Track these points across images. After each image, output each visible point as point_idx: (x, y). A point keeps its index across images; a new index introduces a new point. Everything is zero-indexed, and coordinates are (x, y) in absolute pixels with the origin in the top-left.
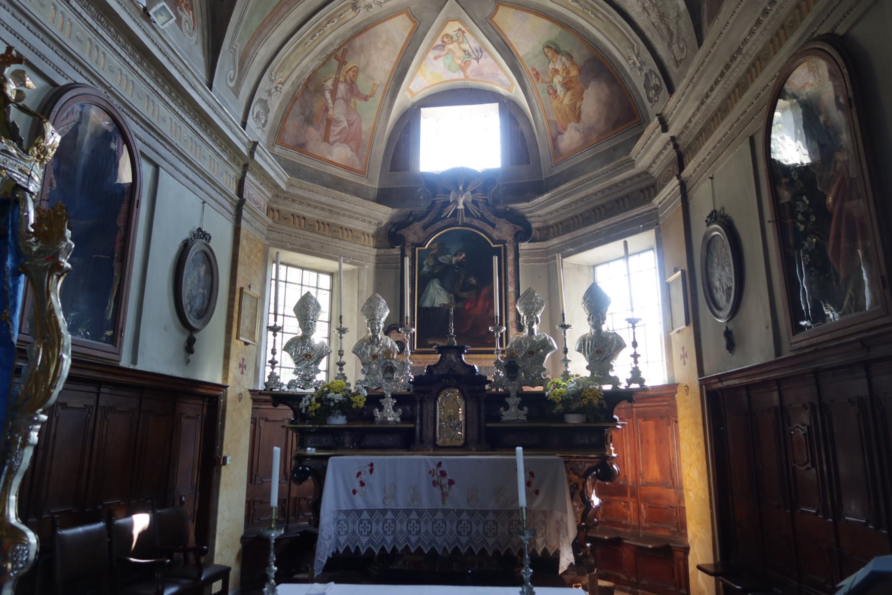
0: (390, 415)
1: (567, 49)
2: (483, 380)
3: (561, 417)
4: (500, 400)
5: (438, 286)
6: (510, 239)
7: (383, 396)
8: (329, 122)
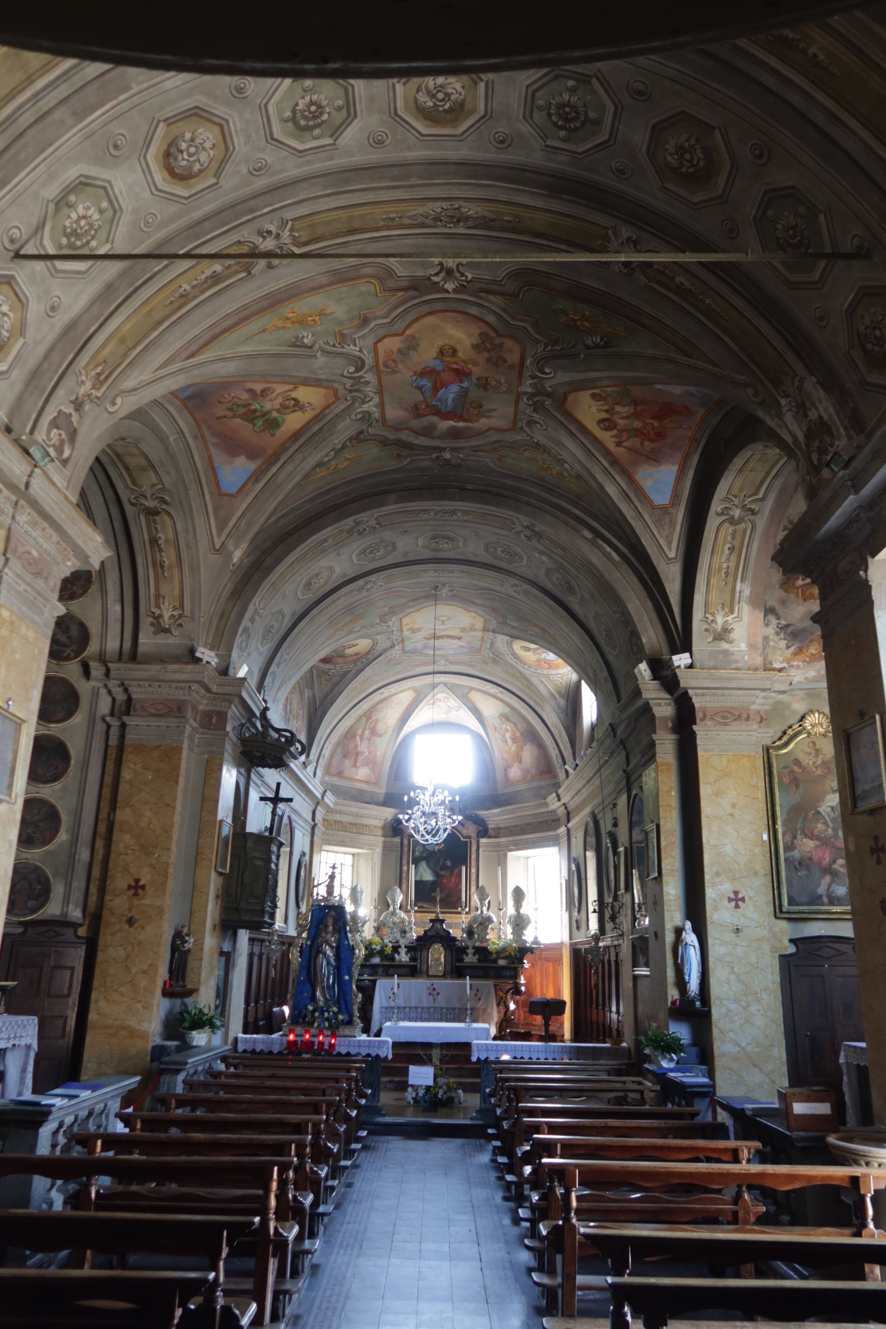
0: (403, 957)
1: (514, 720)
2: (454, 939)
3: (495, 961)
4: (463, 950)
5: (425, 866)
6: (474, 835)
7: (400, 947)
8: (357, 754)
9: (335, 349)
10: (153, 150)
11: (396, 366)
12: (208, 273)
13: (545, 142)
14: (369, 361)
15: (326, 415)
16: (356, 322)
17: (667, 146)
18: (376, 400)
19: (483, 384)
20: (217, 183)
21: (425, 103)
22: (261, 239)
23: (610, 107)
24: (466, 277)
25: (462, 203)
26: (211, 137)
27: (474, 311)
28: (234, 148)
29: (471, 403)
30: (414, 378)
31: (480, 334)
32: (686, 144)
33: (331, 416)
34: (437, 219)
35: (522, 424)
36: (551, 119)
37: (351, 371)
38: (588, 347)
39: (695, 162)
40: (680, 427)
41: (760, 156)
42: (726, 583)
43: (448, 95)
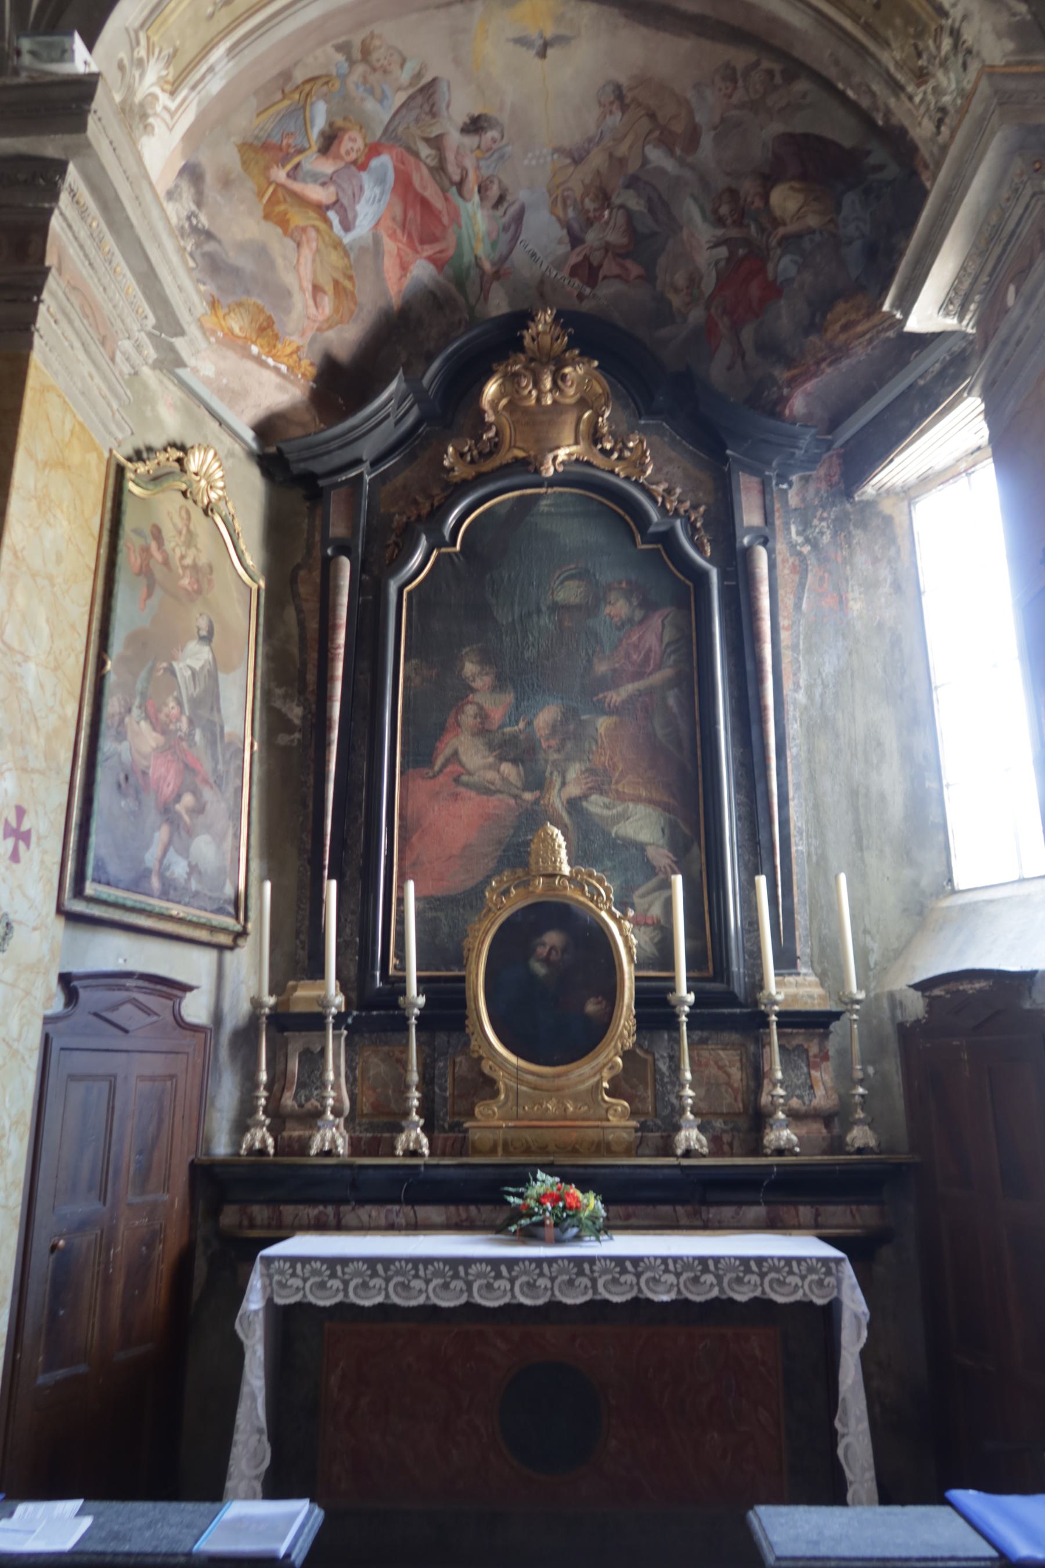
42: (212, 16)
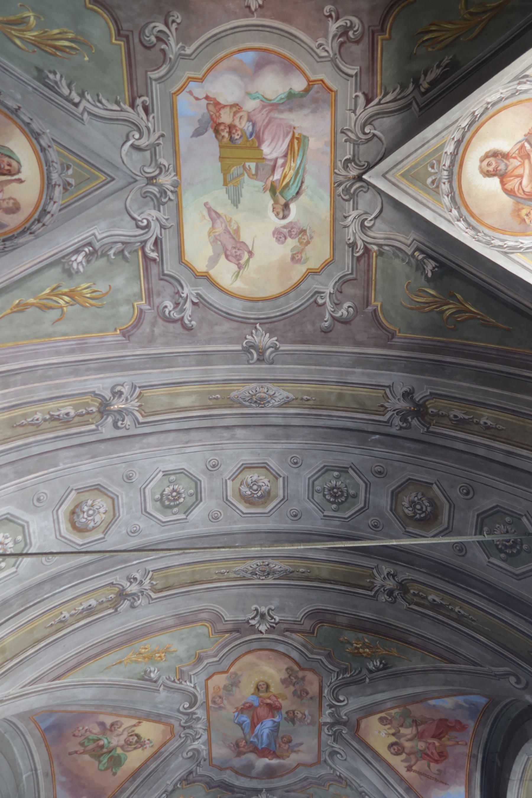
9: (175, 684)
10: (64, 507)
11: (222, 702)
12: (85, 605)
13: (323, 513)
14: (201, 697)
15: (162, 753)
16: (193, 660)
17: (403, 503)
18: (205, 737)
19: (292, 718)
20: (104, 538)
21: (246, 492)
22: (129, 584)
23: (362, 485)
24: (275, 619)
25: (270, 560)
26: (105, 505)
27: (281, 648)
28: (119, 516)
29: (282, 738)
30: (236, 714)
31: (287, 669)
32: (416, 499)
33: (166, 754)
34: (254, 573)
35: (325, 756)
36: (325, 498)
37: (186, 706)
38: (371, 671)
39: (424, 510)
40: (458, 743)
41: (468, 493)
43: (260, 487)
